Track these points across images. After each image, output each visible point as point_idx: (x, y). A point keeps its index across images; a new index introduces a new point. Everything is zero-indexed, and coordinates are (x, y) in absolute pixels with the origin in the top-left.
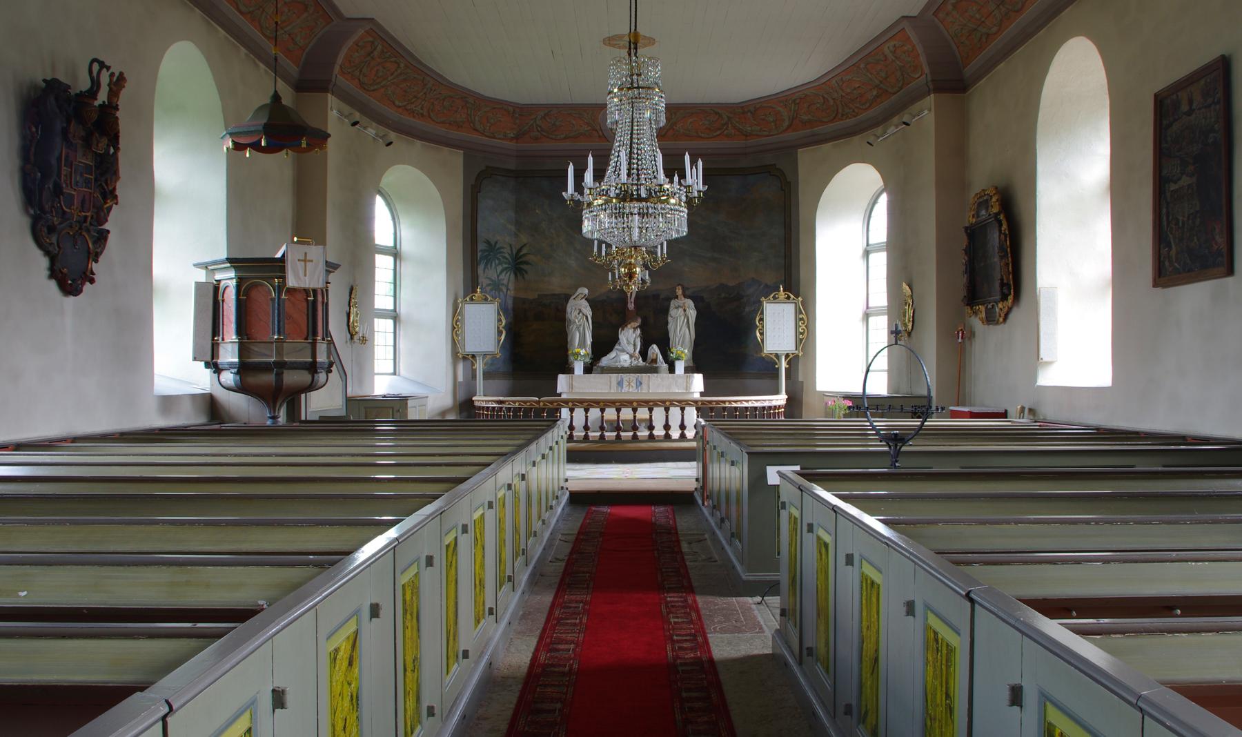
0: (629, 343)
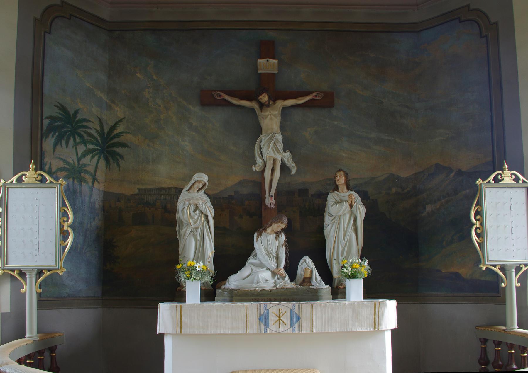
0: (269, 254)
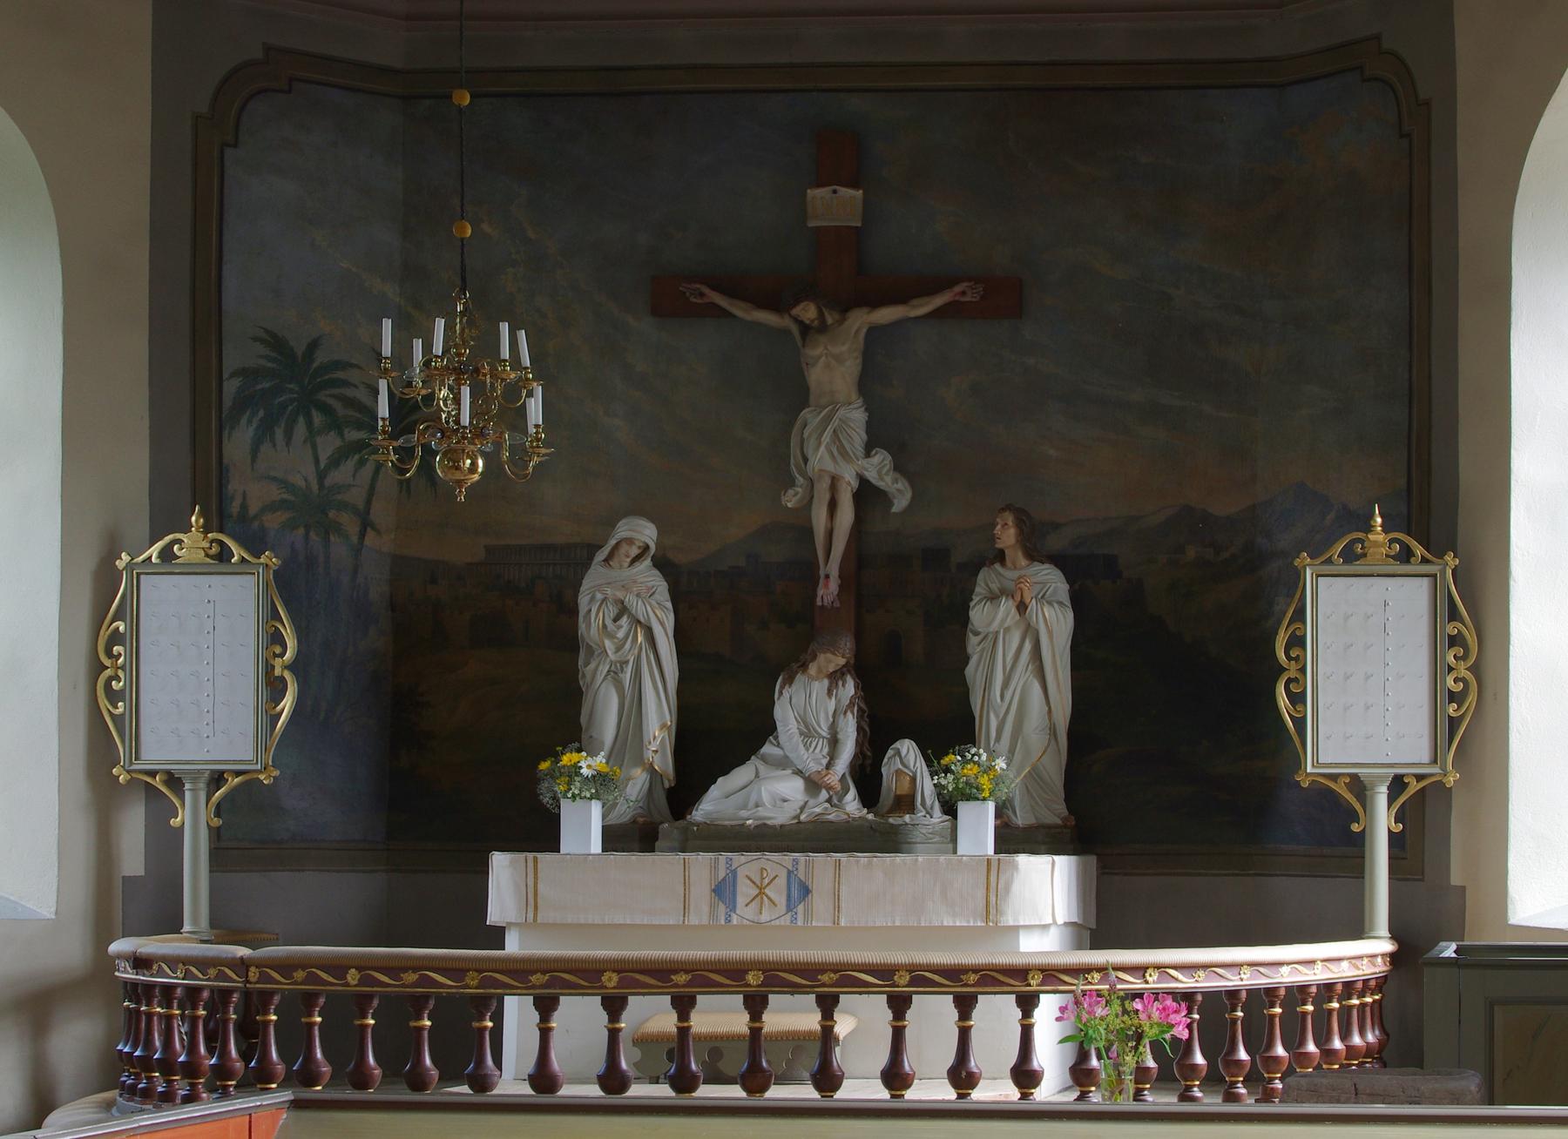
0: (808, 733)
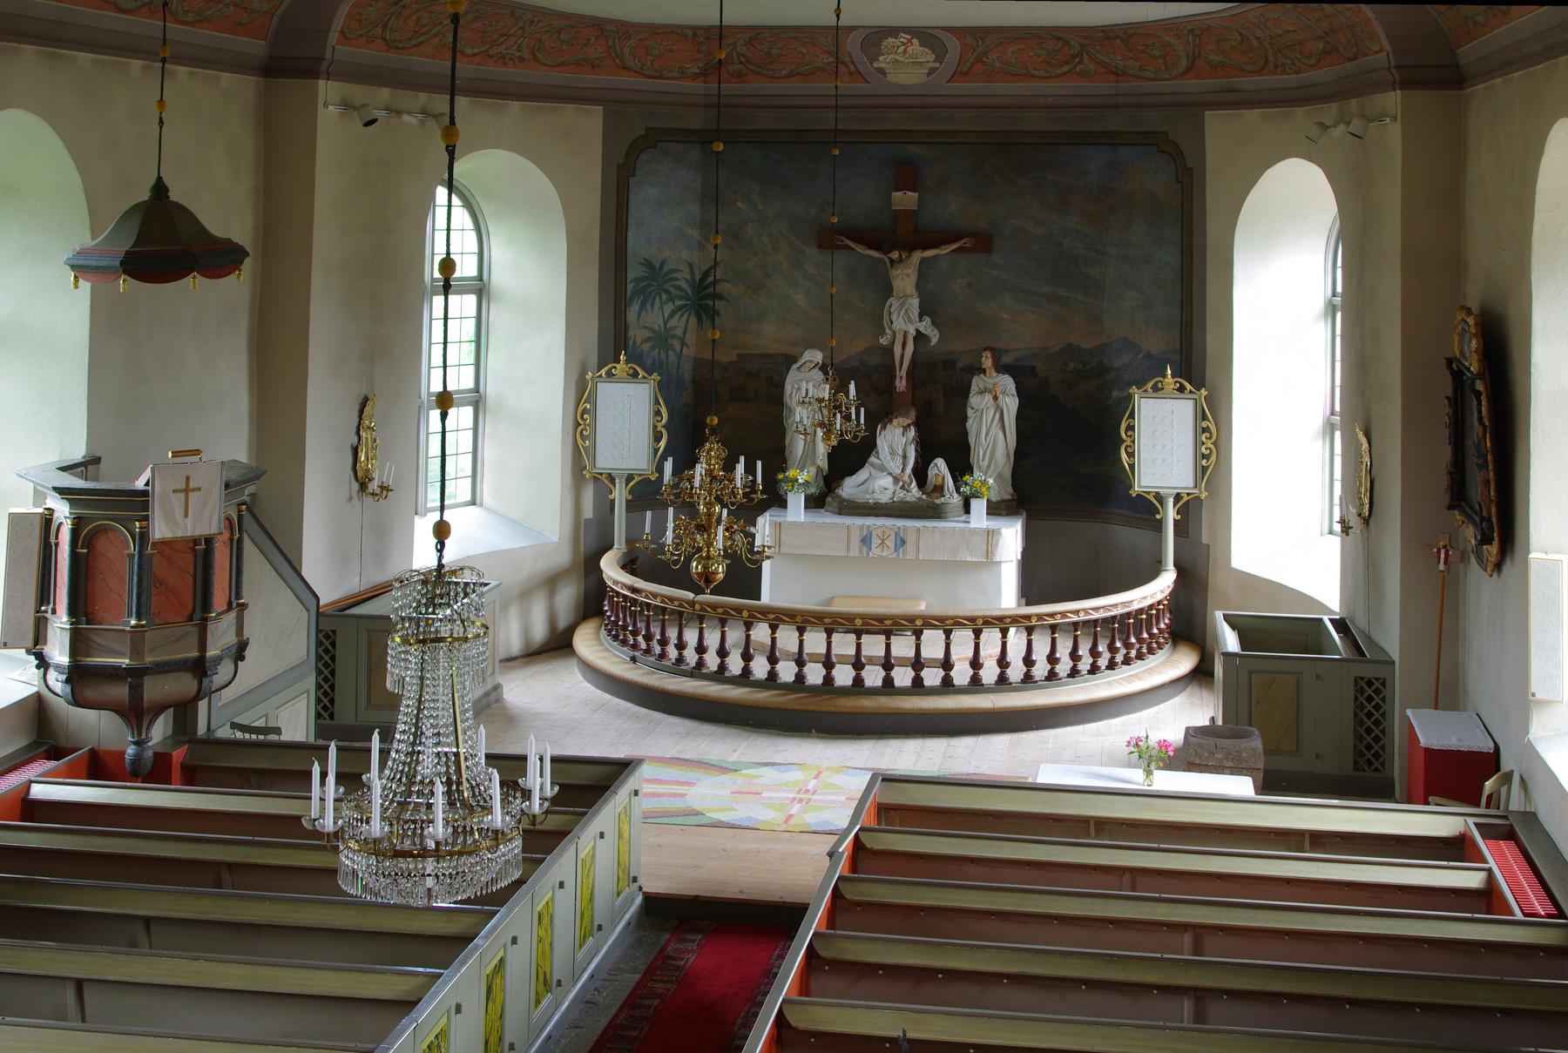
0: (893, 453)
